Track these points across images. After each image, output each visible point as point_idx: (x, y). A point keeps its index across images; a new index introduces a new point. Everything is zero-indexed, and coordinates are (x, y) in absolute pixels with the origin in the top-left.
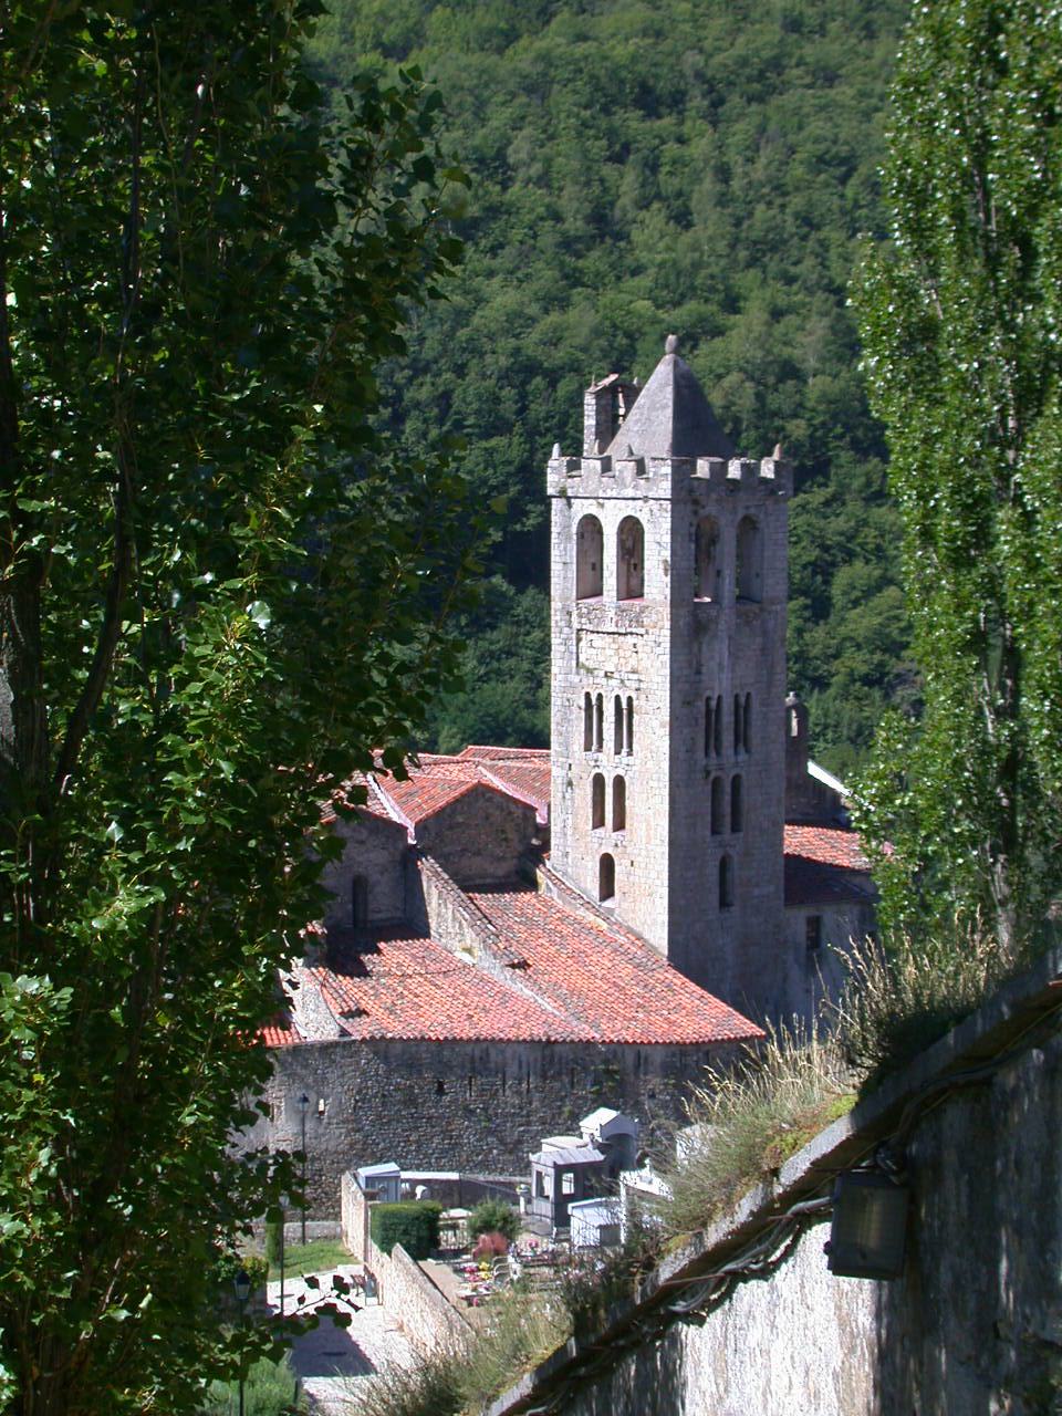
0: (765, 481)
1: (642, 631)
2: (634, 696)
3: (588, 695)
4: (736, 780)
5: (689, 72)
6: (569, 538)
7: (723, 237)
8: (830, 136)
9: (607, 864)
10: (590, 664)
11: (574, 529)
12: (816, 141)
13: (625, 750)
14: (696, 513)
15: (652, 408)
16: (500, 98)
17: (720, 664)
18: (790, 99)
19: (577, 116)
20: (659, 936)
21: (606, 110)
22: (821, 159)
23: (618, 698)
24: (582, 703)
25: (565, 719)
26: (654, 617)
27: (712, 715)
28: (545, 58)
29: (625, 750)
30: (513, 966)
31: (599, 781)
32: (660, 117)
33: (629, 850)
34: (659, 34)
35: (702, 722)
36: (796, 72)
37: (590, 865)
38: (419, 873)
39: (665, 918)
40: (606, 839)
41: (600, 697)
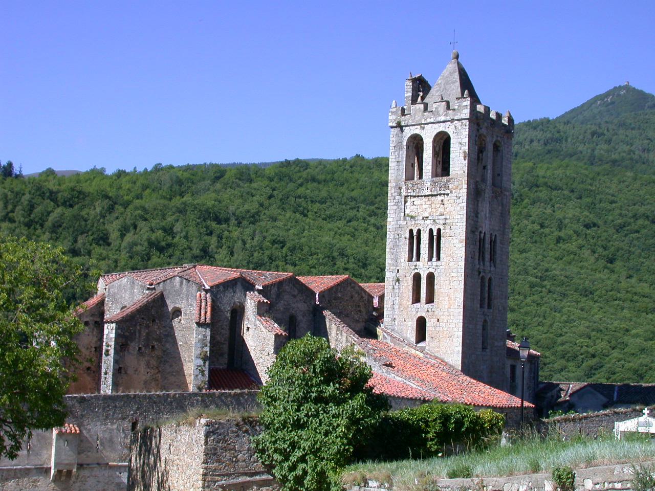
0: (503, 125)
1: (447, 192)
2: (442, 228)
3: (411, 231)
4: (490, 279)
5: (230, 212)
6: (401, 148)
7: (245, 260)
8: (277, 234)
9: (421, 324)
10: (413, 214)
11: (405, 143)
12: (273, 235)
13: (435, 258)
14: (478, 130)
15: (447, 83)
16: (170, 213)
17: (486, 215)
18: (263, 224)
19: (196, 221)
20: (456, 360)
21: (204, 220)
22: (274, 241)
23: (431, 231)
24: (407, 236)
25: (396, 245)
26: (456, 184)
27: (482, 241)
28: (184, 203)
29: (435, 258)
30: (386, 365)
31: (417, 278)
32: (222, 224)
33: (436, 313)
34: (220, 202)
35: (478, 243)
36: (264, 217)
37: (410, 324)
38: (324, 318)
39: (460, 349)
40: (422, 309)
41: (419, 231)
